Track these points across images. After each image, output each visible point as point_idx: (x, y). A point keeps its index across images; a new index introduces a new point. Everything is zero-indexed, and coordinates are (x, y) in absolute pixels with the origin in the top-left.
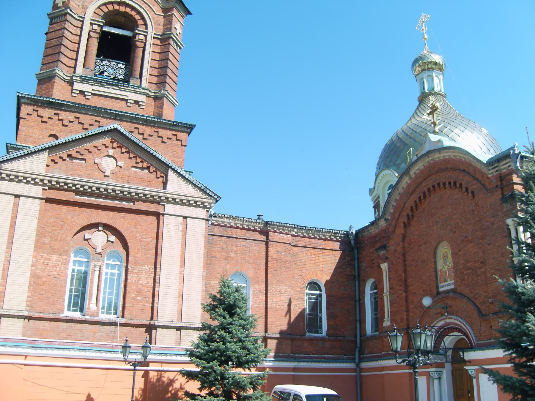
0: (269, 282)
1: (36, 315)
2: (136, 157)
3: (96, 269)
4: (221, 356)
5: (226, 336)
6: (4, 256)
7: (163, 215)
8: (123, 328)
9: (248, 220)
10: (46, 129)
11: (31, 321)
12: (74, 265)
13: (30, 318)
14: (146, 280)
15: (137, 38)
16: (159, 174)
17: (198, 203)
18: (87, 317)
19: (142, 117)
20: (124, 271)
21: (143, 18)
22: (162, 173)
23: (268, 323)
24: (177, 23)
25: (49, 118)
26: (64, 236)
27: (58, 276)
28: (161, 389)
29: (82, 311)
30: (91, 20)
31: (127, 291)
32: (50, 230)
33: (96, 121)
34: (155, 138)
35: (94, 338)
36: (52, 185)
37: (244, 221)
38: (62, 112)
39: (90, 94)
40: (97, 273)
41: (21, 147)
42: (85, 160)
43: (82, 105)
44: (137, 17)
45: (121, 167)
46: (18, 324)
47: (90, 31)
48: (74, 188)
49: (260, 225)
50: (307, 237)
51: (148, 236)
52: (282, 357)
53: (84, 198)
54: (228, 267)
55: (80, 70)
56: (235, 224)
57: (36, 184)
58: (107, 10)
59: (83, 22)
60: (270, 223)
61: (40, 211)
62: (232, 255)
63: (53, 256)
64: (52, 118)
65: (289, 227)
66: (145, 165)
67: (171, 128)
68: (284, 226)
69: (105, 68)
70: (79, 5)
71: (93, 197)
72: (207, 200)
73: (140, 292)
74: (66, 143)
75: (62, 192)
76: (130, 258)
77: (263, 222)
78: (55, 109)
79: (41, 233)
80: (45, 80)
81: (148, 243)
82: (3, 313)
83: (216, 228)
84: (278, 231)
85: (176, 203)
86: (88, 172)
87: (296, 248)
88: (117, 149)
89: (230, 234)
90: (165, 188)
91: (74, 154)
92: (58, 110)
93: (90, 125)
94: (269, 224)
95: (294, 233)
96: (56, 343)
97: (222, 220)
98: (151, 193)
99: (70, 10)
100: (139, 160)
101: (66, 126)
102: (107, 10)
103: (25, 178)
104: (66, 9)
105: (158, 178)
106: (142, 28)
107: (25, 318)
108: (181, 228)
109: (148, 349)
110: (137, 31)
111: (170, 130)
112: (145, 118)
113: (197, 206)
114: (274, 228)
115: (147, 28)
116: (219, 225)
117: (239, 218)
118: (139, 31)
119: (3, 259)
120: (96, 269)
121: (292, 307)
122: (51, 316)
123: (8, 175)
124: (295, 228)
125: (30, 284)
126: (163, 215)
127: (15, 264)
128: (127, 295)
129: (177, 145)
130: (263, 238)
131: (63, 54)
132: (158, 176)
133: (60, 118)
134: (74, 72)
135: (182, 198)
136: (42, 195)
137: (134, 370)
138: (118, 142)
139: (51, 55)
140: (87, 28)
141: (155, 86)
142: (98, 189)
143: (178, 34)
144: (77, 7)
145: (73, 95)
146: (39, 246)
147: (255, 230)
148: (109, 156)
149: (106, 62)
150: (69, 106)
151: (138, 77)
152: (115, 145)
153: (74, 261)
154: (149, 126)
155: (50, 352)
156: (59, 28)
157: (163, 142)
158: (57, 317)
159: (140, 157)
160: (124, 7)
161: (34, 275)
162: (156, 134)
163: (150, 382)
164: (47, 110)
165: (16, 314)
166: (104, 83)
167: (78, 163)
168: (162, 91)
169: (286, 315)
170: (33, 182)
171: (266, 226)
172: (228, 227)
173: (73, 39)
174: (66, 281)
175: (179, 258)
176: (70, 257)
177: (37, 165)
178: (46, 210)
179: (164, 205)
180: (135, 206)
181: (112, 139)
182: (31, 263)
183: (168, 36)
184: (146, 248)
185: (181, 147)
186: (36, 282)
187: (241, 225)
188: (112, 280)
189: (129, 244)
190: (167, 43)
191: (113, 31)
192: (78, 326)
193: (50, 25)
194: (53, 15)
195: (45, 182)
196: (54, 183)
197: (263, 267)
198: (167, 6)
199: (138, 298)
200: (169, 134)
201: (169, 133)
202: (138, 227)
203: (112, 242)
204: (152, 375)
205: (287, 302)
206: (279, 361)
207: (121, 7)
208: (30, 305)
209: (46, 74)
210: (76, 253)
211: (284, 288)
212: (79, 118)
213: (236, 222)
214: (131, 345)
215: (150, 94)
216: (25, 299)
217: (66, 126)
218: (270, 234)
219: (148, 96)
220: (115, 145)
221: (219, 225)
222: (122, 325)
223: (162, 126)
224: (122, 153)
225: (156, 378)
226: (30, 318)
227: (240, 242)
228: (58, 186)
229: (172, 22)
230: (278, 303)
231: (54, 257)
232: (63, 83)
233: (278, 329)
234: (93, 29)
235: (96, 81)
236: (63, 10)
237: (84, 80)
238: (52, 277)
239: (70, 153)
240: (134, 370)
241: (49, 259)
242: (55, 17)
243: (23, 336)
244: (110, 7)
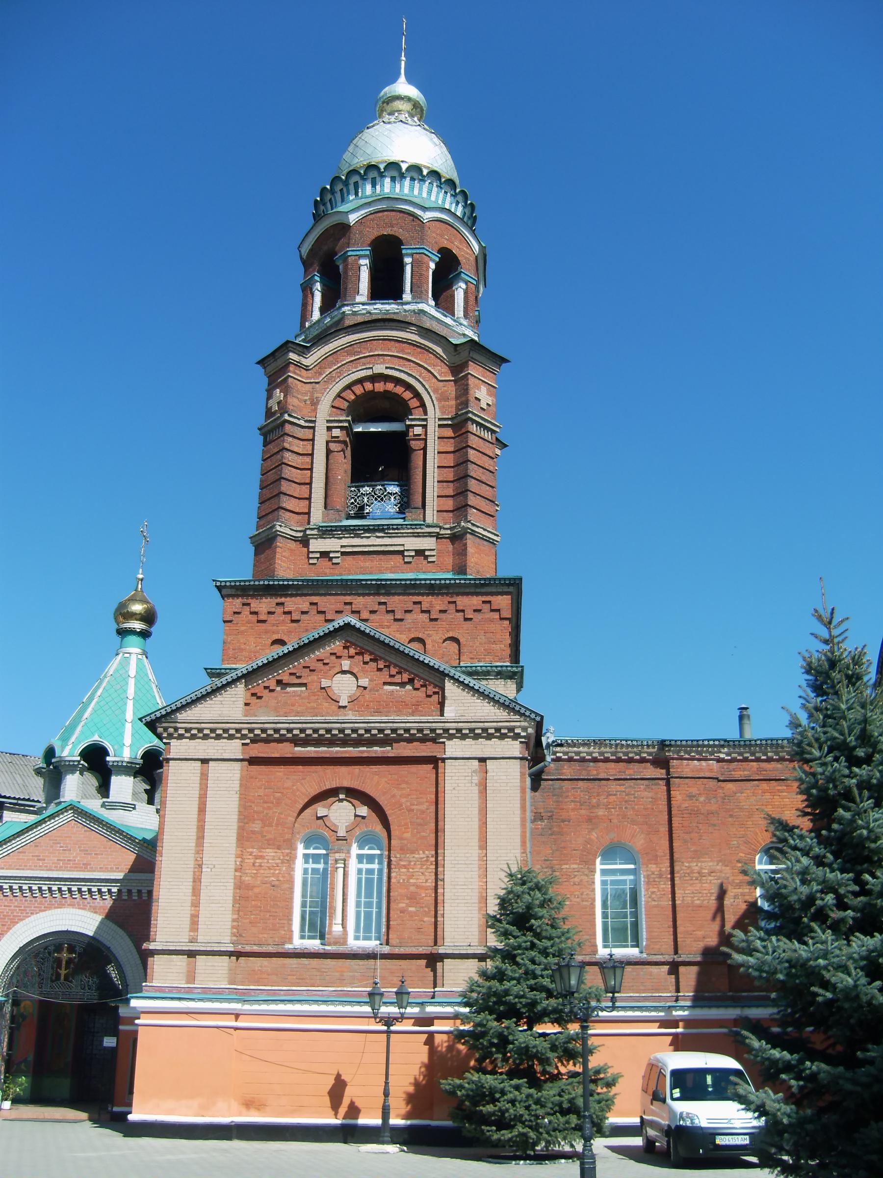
0: (676, 856)
1: (248, 948)
2: (388, 667)
3: (338, 865)
4: (499, 1002)
5: (506, 969)
6: (193, 859)
7: (443, 760)
8: (389, 963)
9: (624, 742)
10: (266, 632)
11: (242, 959)
12: (307, 862)
13: (238, 955)
14: (423, 877)
15: (411, 434)
16: (431, 689)
17: (503, 731)
18: (327, 948)
19: (423, 582)
20: (386, 863)
21: (417, 395)
22: (435, 686)
23: (679, 935)
24: (479, 389)
25: (269, 613)
26: (283, 816)
27: (277, 883)
28: (455, 1064)
29: (322, 937)
30: (328, 421)
31: (392, 898)
32: (261, 809)
33: (346, 604)
34: (452, 615)
35: (341, 981)
36: (255, 735)
37: (617, 745)
38: (288, 599)
39: (339, 555)
40: (341, 871)
41: (223, 671)
42: (305, 685)
43: (313, 580)
44: (407, 395)
45: (365, 688)
46: (220, 964)
47: (327, 442)
48: (290, 735)
49: (651, 750)
50: (752, 761)
51: (421, 800)
52: (709, 999)
53: (309, 749)
54: (594, 835)
55: (317, 516)
56: (601, 754)
57: (231, 737)
58: (353, 397)
59: (313, 428)
60: (667, 743)
61: (241, 780)
62: (601, 812)
63: (268, 850)
64: (273, 613)
65: (709, 746)
66: (406, 677)
67: (478, 590)
68: (698, 746)
69: (366, 499)
70: (305, 401)
71: (324, 745)
72: (518, 724)
73: (413, 898)
74: (269, 663)
75: (272, 744)
76: (394, 842)
77: (655, 743)
78: (276, 595)
79: (245, 816)
80: (264, 544)
81: (423, 812)
82: (198, 949)
83: (566, 765)
84: (687, 756)
85: (464, 737)
86: (312, 704)
87: (730, 785)
88: (357, 657)
89: (593, 774)
90: (442, 715)
91: (286, 678)
92: (281, 596)
93: (336, 612)
94: (667, 746)
95: (722, 756)
96: (282, 993)
97: (575, 749)
98: (417, 725)
99: (290, 415)
100: (394, 671)
101: (298, 621)
102: (353, 397)
103: (213, 730)
104: (282, 415)
105: (430, 696)
106: (417, 414)
107: (230, 954)
108: (476, 779)
109: (405, 996)
110: (408, 423)
111: (477, 594)
112: (428, 582)
113: (503, 737)
114: (679, 751)
115: (426, 413)
116: (570, 760)
117: (608, 742)
118: (412, 420)
119: (191, 864)
120: (338, 865)
121: (727, 902)
122: (271, 949)
123: (188, 730)
124: (723, 746)
125: (235, 901)
126: (443, 760)
127: (209, 870)
128: (392, 905)
129: (492, 621)
130: (661, 773)
131: (285, 494)
132: (430, 692)
133: (286, 609)
134: (309, 523)
135: (473, 725)
136: (243, 753)
137: (388, 1033)
138: (356, 646)
139: (269, 499)
140: (321, 437)
141: (451, 515)
142: (328, 731)
143: (485, 407)
144: (302, 405)
145: (311, 561)
146: (244, 837)
147: (643, 761)
148: (344, 672)
149: (367, 488)
150: (297, 587)
151: (420, 505)
152: (352, 651)
153: (306, 857)
154: (438, 595)
155: (289, 1007)
156: (276, 450)
157: (466, 619)
158: (280, 949)
159: (396, 666)
160: (382, 383)
161: (240, 885)
162: (452, 606)
163: (437, 1052)
164: (264, 600)
165: (215, 949)
166: (359, 530)
167: (294, 692)
168: (463, 524)
169: (714, 918)
170: (226, 735)
171: (663, 749)
172: (589, 761)
173: (302, 463)
174: (291, 889)
175: (477, 833)
176: (296, 849)
177: (231, 706)
178: (252, 778)
179: (444, 743)
180: (394, 751)
181: (347, 641)
182: (233, 867)
183: (463, 418)
184: (418, 821)
185: (501, 622)
186: (244, 895)
187: (613, 754)
188: (369, 882)
189: (390, 818)
190: (463, 430)
191: (372, 430)
192: (315, 962)
193: (264, 446)
194: (266, 429)
195: (245, 732)
196: (257, 732)
197: (664, 829)
198: (458, 360)
199: (410, 909)
200: (475, 602)
201: (476, 601)
202: (403, 786)
203: (363, 818)
204: (438, 1039)
205: (715, 891)
206: (702, 1007)
207: (376, 385)
208: (238, 933)
209: (264, 535)
210: (308, 844)
211: (707, 865)
212: (316, 604)
213: (602, 749)
214: (410, 990)
215: (443, 532)
216: (229, 924)
217: (298, 621)
218: (674, 763)
219: (438, 536)
220: (352, 651)
221: (570, 760)
222: (384, 956)
223: (462, 590)
224: (365, 663)
225: (445, 1044)
226: (238, 955)
227: (614, 787)
228: (264, 735)
229: (467, 389)
230: (697, 894)
231: (270, 852)
232: (293, 545)
233: (701, 945)
234: (333, 437)
235: (346, 530)
236: (279, 418)
237: (326, 532)
238: (268, 885)
239: (279, 678)
240: (388, 1033)
241: (262, 857)
242: (271, 431)
243: (188, 983)
244: (358, 390)
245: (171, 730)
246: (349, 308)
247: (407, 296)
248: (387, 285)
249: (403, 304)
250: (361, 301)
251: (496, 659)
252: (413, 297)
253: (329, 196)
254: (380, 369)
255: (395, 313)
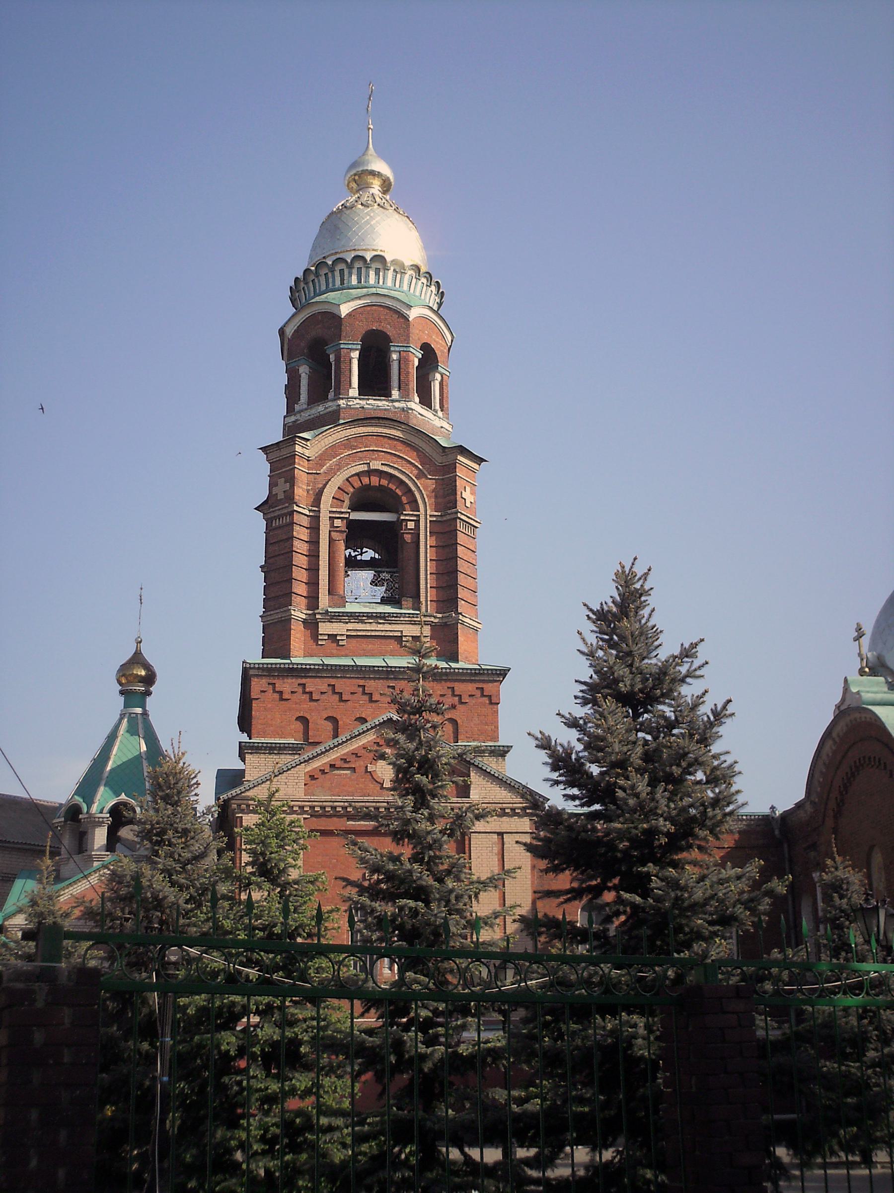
10: (290, 709)
78: (297, 677)
108: (496, 849)
111: (471, 681)
118: (406, 515)
133: (307, 690)
185: (491, 706)
201: (471, 687)
242: (275, 518)
245: (244, 806)
246: (344, 401)
247: (395, 394)
248: (375, 381)
249: (393, 401)
250: (353, 398)
251: (489, 738)
252: (401, 396)
253: (312, 277)
254: (376, 465)
255: (385, 410)
